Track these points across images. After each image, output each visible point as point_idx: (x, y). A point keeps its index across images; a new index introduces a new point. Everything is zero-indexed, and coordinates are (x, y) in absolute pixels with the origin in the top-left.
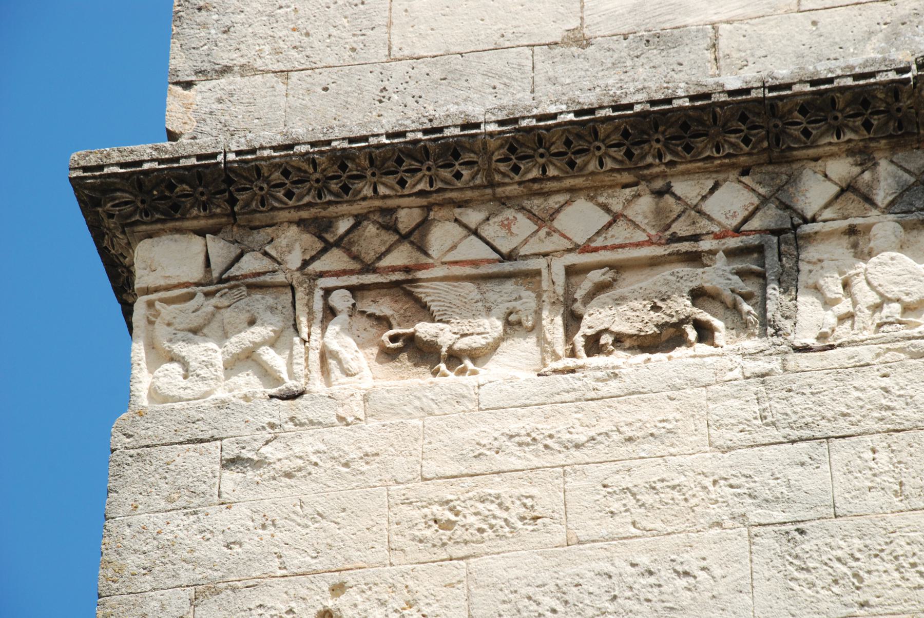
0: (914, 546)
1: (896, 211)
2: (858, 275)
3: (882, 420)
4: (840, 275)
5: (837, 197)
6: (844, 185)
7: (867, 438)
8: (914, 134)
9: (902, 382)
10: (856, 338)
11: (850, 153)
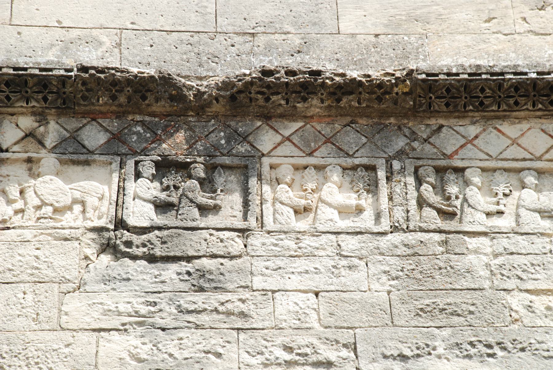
0: (39, 352)
1: (57, 152)
2: (29, 187)
3: (32, 275)
4: (19, 186)
5: (23, 139)
6: (28, 132)
7: (22, 285)
8: (71, 108)
9: (48, 253)
10: (24, 225)
11: (34, 114)
